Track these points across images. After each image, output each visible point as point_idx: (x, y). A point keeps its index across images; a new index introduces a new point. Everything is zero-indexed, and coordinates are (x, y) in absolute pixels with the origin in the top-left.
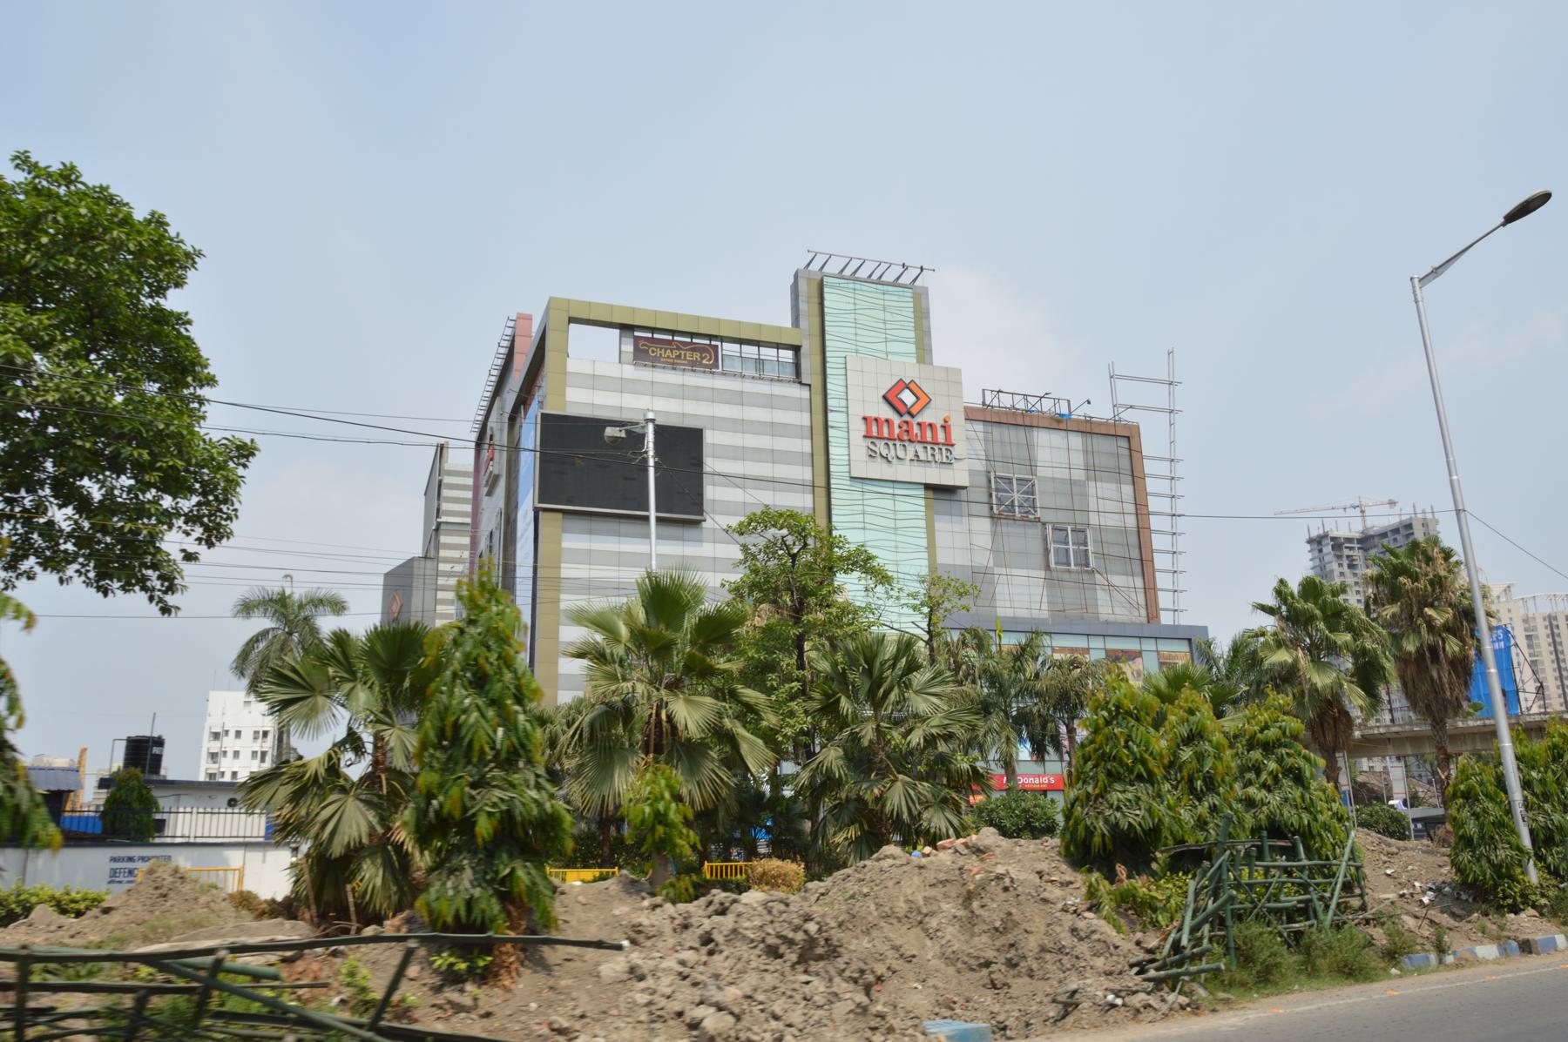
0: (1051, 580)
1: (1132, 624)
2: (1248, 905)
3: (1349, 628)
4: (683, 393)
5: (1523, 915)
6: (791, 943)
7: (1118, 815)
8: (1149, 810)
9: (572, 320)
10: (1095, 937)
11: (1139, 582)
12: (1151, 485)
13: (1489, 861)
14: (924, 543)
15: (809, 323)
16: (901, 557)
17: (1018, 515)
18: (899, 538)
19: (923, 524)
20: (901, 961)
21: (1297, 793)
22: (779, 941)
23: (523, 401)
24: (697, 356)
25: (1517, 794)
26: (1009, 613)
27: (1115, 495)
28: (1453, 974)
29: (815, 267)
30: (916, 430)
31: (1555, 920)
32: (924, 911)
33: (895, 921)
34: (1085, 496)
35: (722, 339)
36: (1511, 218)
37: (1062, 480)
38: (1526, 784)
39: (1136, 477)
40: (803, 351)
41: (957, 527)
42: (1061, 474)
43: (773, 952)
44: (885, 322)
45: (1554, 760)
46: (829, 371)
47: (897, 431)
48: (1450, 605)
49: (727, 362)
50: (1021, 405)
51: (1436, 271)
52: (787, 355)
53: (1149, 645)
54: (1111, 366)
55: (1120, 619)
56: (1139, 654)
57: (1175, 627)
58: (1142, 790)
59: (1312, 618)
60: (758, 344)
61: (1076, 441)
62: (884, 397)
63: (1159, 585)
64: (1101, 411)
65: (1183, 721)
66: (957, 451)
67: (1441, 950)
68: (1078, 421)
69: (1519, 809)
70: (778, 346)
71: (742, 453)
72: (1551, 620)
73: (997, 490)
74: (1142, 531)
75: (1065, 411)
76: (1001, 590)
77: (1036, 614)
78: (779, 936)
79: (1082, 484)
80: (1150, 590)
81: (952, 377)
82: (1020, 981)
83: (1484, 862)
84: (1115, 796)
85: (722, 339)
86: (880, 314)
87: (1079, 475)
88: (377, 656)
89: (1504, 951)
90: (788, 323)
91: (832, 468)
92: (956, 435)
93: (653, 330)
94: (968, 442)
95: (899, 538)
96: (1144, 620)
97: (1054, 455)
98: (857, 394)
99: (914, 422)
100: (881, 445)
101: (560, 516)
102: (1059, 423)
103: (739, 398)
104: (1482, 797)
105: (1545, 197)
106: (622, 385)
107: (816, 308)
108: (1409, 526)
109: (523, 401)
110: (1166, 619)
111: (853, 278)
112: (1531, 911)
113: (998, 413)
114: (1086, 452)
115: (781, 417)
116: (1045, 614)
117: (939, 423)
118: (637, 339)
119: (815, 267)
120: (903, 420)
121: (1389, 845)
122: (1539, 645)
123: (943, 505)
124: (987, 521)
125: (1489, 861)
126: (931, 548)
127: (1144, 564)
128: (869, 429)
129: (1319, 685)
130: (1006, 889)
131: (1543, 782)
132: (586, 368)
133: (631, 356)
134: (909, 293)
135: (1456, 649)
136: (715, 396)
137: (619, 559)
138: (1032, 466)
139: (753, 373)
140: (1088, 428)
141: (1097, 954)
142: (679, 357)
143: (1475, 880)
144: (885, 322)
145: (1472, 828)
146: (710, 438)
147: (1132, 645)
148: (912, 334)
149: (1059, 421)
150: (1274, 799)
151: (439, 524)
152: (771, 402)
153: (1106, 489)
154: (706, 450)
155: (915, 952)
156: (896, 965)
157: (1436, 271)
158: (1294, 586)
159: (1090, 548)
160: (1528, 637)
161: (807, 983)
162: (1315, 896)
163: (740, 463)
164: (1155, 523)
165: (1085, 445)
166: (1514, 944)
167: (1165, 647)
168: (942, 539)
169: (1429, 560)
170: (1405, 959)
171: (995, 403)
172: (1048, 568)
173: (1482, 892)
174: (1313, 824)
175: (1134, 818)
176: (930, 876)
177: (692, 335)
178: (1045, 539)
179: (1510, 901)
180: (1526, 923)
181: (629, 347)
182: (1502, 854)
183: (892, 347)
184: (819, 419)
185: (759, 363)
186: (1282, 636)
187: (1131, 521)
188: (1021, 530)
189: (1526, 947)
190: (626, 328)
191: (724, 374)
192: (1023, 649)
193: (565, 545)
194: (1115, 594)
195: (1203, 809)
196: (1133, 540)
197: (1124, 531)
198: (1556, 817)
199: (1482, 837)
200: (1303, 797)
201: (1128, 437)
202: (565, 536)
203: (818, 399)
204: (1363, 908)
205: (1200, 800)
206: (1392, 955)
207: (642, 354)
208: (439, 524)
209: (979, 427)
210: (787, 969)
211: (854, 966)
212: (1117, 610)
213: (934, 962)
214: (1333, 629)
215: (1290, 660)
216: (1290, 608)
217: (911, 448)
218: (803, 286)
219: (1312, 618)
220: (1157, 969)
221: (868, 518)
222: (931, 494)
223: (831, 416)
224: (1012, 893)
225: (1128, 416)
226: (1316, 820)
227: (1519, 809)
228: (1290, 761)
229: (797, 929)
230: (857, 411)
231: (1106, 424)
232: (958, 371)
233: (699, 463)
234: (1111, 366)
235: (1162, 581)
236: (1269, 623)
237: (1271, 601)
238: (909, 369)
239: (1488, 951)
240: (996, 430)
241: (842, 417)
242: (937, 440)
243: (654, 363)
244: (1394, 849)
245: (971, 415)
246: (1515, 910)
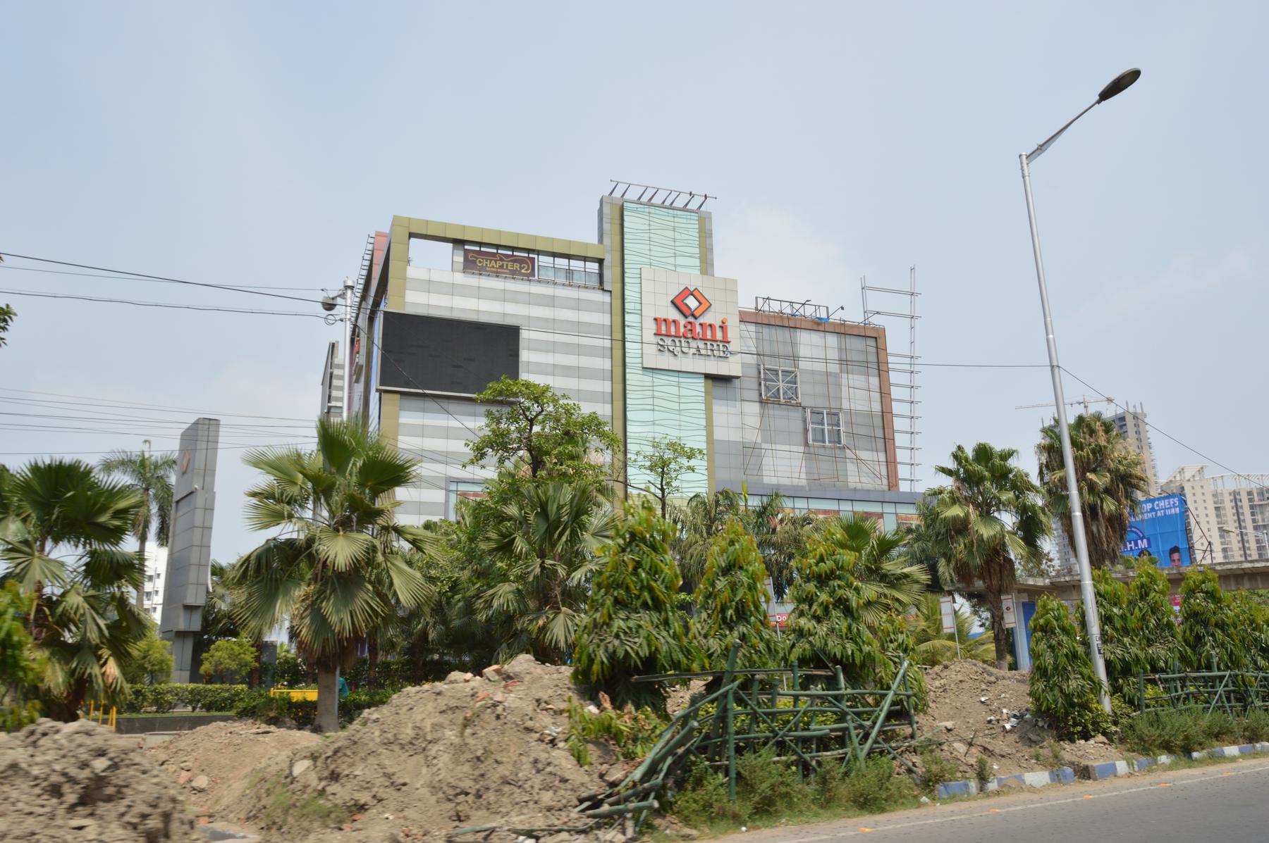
0: (809, 455)
1: (875, 491)
2: (767, 734)
3: (1014, 487)
4: (504, 297)
5: (1092, 742)
6: (72, 780)
7: (617, 642)
8: (648, 639)
9: (411, 235)
10: (549, 769)
11: (882, 457)
12: (894, 377)
13: (1061, 690)
14: (703, 422)
15: (611, 240)
17: (782, 400)
18: (683, 418)
19: (703, 406)
20: (391, 790)
21: (843, 624)
22: (62, 779)
23: (376, 304)
24: (517, 266)
25: (1095, 629)
26: (774, 481)
27: (864, 385)
28: (996, 800)
29: (617, 194)
30: (698, 329)
31: (1123, 747)
32: (429, 738)
33: (396, 748)
34: (839, 386)
35: (539, 253)
36: (1106, 94)
37: (820, 373)
38: (1106, 619)
40: (605, 263)
41: (732, 410)
42: (809, 367)
43: (56, 791)
45: (1142, 598)
46: (627, 280)
47: (682, 330)
48: (1109, 471)
49: (542, 272)
50: (788, 310)
51: (1041, 148)
52: (593, 267)
53: (889, 509)
54: (863, 279)
55: (866, 487)
57: (911, 494)
58: (646, 619)
59: (981, 479)
60: (569, 257)
61: (832, 340)
63: (899, 459)
64: (854, 316)
65: (723, 551)
66: (731, 347)
67: (983, 778)
68: (834, 324)
69: (1096, 641)
70: (585, 259)
71: (553, 348)
72: (1235, 495)
73: (765, 380)
74: (886, 414)
75: (824, 316)
76: (767, 461)
77: (796, 482)
78: (65, 774)
79: (837, 376)
80: (891, 463)
81: (730, 286)
82: (480, 813)
83: (1057, 692)
84: (618, 623)
85: (539, 253)
86: (671, 234)
87: (834, 368)
88: (33, 491)
89: (1057, 778)
90: (594, 239)
91: (628, 360)
92: (732, 334)
93: (481, 244)
94: (741, 338)
95: (683, 418)
96: (886, 488)
97: (814, 350)
98: (650, 299)
99: (697, 322)
100: (668, 341)
101: (398, 396)
103: (552, 302)
104: (1057, 630)
105: (1134, 75)
106: (453, 289)
107: (618, 227)
108: (1123, 419)
109: (376, 304)
110: (904, 487)
111: (649, 203)
112: (1100, 738)
113: (768, 316)
114: (840, 349)
115: (586, 317)
116: (803, 482)
117: (718, 323)
118: (467, 251)
119: (617, 194)
120: (688, 321)
121: (990, 674)
122: (1225, 515)
123: (720, 390)
124: (757, 405)
125: (1061, 690)
126: (709, 426)
127: (887, 442)
128: (659, 328)
129: (985, 536)
130: (498, 717)
131: (1123, 617)
132: (423, 275)
133: (461, 266)
134: (695, 216)
135: (1113, 508)
136: (531, 299)
137: (447, 433)
138: (795, 358)
139: (564, 281)
140: (843, 330)
141: (547, 788)
142: (501, 267)
143: (1049, 709)
145: (1048, 660)
146: (524, 334)
148: (697, 251)
149: (818, 324)
150: (822, 629)
151: (330, 408)
152: (578, 305)
153: (857, 380)
154: (522, 344)
155: (407, 780)
156: (382, 793)
157: (1041, 148)
158: (969, 452)
159: (842, 429)
160: (1217, 509)
161: (80, 828)
162: (851, 725)
163: (551, 355)
164: (897, 408)
165: (840, 343)
166: (1069, 770)
168: (718, 420)
169: (1092, 432)
170: (940, 787)
171: (766, 308)
172: (806, 444)
173: (1057, 719)
174: (857, 654)
175: (637, 647)
176: (442, 702)
177: (513, 249)
178: (805, 421)
179: (1079, 729)
180: (1092, 750)
181: (460, 258)
182: (1074, 684)
183: (680, 261)
184: (618, 319)
185: (569, 273)
186: (957, 494)
187: (877, 407)
188: (785, 413)
189: (1084, 773)
190: (458, 243)
191: (539, 281)
192: (765, 508)
193: (402, 420)
194: (862, 466)
195: (733, 638)
196: (878, 422)
197: (871, 414)
198: (1134, 650)
199: (1056, 668)
200: (849, 628)
201: (875, 337)
202: (402, 413)
203: (617, 303)
204: (912, 736)
205: (731, 629)
206: (929, 783)
207: (470, 265)
208: (330, 408)
209: (752, 328)
210: (61, 811)
211: (136, 810)
212: (863, 479)
213: (422, 791)
214: (1001, 488)
215: (962, 515)
216: (966, 471)
217: (693, 344)
218: (606, 210)
219: (981, 479)
220: (611, 805)
221: (657, 402)
222: (710, 382)
223: (627, 317)
224: (501, 722)
225: (876, 320)
226: (861, 650)
227: (1096, 641)
228: (840, 592)
229: (84, 765)
230: (649, 313)
231: (857, 327)
232: (735, 281)
233: (516, 355)
234: (863, 279)
235: (902, 456)
236: (948, 483)
237: (952, 465)
238: (693, 279)
239: (1038, 777)
240: (766, 330)
241: (637, 318)
242: (716, 340)
243: (481, 272)
244: (993, 679)
245: (745, 318)
246: (1086, 736)
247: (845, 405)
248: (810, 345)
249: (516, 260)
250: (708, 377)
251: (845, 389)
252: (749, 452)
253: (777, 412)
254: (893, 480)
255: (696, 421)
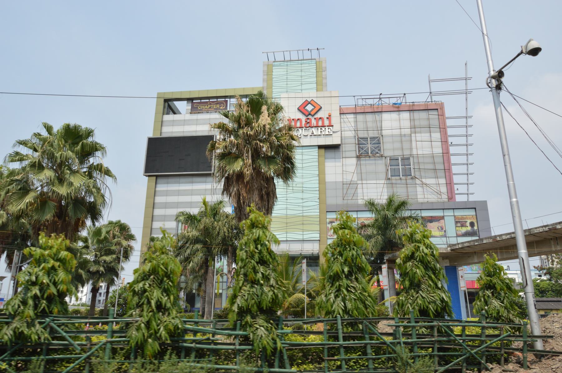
1: (438, 202)
11: (443, 181)
14: (317, 173)
16: (305, 180)
18: (304, 172)
24: (218, 106)
35: (231, 97)
39: (443, 129)
44: (301, 76)
53: (450, 213)
56: (443, 218)
62: (298, 109)
74: (446, 154)
80: (450, 184)
85: (231, 97)
86: (299, 74)
87: (408, 131)
97: (391, 124)
102: (397, 108)
123: (330, 153)
127: (448, 171)
140: (412, 109)
142: (210, 108)
144: (301, 76)
147: (439, 213)
159: (412, 167)
167: (458, 213)
187: (438, 150)
188: (374, 162)
201: (437, 109)
238: (311, 94)
240: (360, 117)
247: (414, 152)
248: (391, 124)
249: (218, 103)
250: (320, 147)
251: (414, 143)
252: (348, 187)
253: (367, 162)
254: (451, 197)
255: (313, 172)
